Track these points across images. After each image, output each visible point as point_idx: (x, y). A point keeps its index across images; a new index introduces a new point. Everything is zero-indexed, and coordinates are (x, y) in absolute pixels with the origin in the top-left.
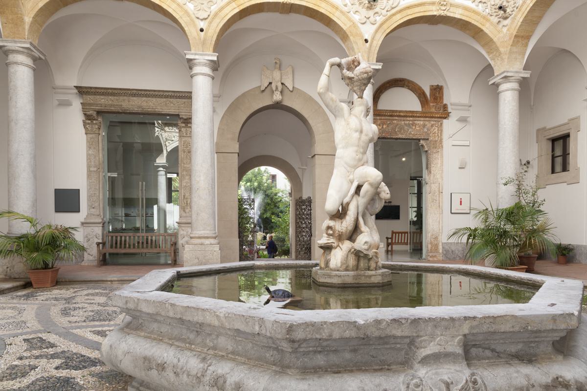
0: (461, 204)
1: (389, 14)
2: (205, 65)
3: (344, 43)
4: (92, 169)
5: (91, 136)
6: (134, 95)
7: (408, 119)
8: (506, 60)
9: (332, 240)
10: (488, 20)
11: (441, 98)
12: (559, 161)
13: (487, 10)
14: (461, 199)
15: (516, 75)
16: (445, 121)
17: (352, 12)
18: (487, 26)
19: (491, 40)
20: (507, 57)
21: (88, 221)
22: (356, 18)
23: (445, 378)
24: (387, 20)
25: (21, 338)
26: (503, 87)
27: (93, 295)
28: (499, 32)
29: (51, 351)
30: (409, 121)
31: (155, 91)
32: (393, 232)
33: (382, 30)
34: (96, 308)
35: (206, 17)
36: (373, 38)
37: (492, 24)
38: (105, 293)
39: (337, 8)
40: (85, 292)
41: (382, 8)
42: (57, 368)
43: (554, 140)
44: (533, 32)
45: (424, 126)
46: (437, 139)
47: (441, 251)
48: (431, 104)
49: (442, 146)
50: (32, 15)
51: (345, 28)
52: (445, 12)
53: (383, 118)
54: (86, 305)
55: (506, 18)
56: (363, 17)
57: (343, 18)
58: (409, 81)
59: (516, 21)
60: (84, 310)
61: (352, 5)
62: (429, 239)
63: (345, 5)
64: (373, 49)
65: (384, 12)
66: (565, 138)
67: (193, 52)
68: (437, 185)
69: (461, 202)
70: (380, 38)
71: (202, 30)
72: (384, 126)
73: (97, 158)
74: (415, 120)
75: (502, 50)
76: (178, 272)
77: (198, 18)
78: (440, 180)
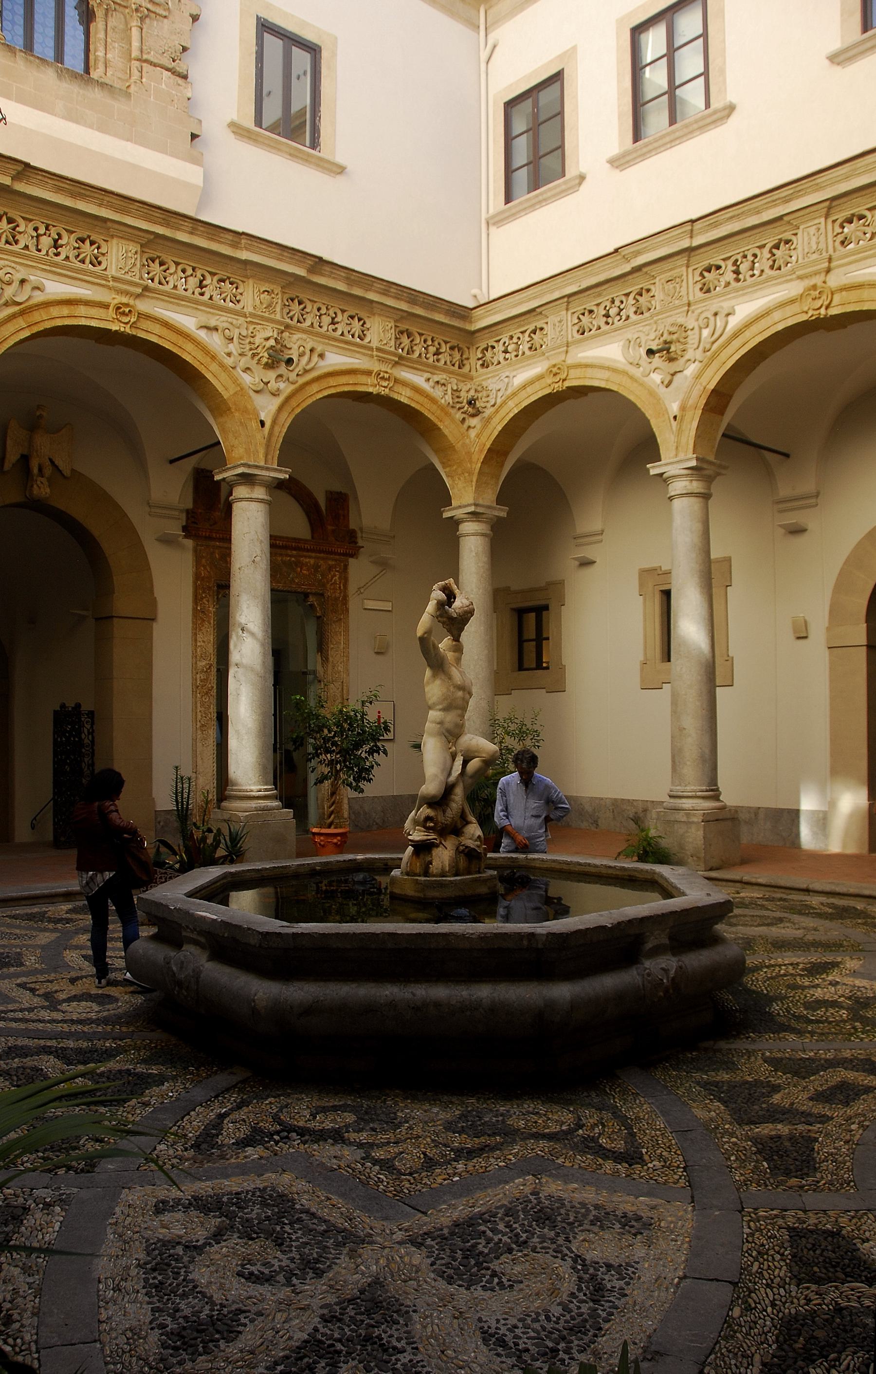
1: (301, 381)
3: (215, 418)
7: (289, 552)
9: (433, 836)
10: (447, 414)
11: (346, 517)
12: (530, 647)
14: (379, 712)
15: (488, 511)
16: (351, 560)
18: (446, 423)
19: (452, 447)
22: (247, 379)
23: (663, 966)
30: (291, 556)
39: (213, 358)
43: (520, 613)
44: (511, 447)
45: (317, 567)
46: (337, 595)
47: (346, 815)
48: (330, 528)
49: (347, 610)
51: (226, 395)
56: (257, 380)
57: (223, 376)
59: (491, 427)
63: (229, 355)
66: (541, 610)
68: (338, 684)
70: (286, 420)
74: (302, 557)
76: (225, 902)
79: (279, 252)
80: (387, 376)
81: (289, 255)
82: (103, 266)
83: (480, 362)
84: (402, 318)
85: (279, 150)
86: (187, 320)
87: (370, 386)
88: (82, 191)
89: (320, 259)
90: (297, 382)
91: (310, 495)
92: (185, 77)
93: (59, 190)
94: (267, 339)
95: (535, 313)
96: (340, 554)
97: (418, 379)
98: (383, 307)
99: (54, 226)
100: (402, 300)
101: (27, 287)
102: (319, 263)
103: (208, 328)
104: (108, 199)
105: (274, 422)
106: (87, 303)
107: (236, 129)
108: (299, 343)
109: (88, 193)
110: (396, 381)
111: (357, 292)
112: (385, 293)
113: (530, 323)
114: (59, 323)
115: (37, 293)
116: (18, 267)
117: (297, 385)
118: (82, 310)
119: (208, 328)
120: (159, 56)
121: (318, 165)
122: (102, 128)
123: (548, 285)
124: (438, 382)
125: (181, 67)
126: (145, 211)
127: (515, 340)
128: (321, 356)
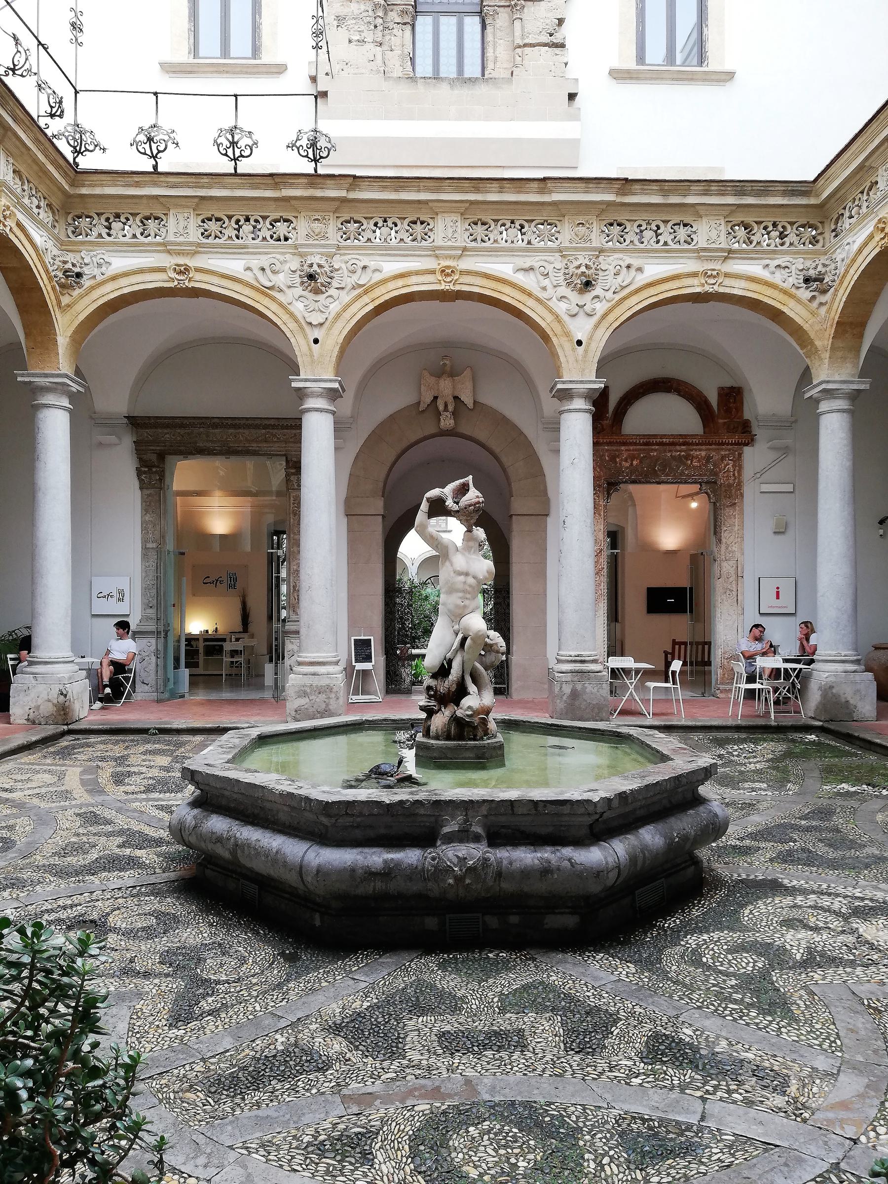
0: (778, 597)
1: (617, 297)
2: (320, 395)
4: (150, 545)
5: (148, 492)
6: (215, 426)
7: (678, 448)
8: (826, 361)
11: (740, 408)
13: (791, 279)
14: (778, 588)
15: (844, 386)
16: (746, 449)
17: (554, 299)
20: (828, 355)
21: (143, 629)
22: (561, 308)
24: (610, 310)
25: (70, 812)
26: (824, 406)
27: (150, 752)
28: (813, 314)
29: (109, 828)
31: (247, 419)
32: (674, 643)
33: (605, 324)
34: (155, 772)
35: (322, 321)
36: (591, 338)
37: (799, 301)
38: (169, 750)
39: (530, 295)
40: (142, 749)
41: (606, 288)
42: (119, 846)
48: (721, 421)
49: (742, 495)
50: (69, 334)
52: (716, 287)
53: (631, 448)
54: (144, 769)
55: (824, 292)
57: (540, 309)
58: (680, 382)
60: (142, 776)
61: (555, 287)
62: (718, 660)
63: (544, 289)
64: (590, 354)
65: (609, 295)
67: (302, 376)
69: (778, 593)
71: (316, 341)
72: (635, 463)
73: (158, 528)
75: (818, 343)
77: (310, 324)
78: (738, 555)
79: (584, 185)
80: (715, 273)
81: (595, 186)
82: (430, 240)
83: (834, 234)
84: (732, 212)
85: (662, 79)
87: (696, 286)
88: (402, 184)
89: (626, 180)
91: (700, 394)
92: (562, 46)
94: (579, 267)
95: (866, 169)
96: (732, 444)
97: (755, 269)
98: (706, 207)
100: (728, 194)
102: (625, 184)
103: (525, 270)
106: (417, 273)
107: (619, 75)
109: (406, 184)
110: (727, 275)
111: (674, 200)
112: (706, 193)
113: (865, 181)
115: (377, 274)
118: (414, 279)
119: (525, 270)
120: (536, 36)
121: (705, 80)
122: (487, 117)
123: (868, 134)
124: (778, 266)
125: (556, 39)
127: (856, 203)
128: (640, 270)
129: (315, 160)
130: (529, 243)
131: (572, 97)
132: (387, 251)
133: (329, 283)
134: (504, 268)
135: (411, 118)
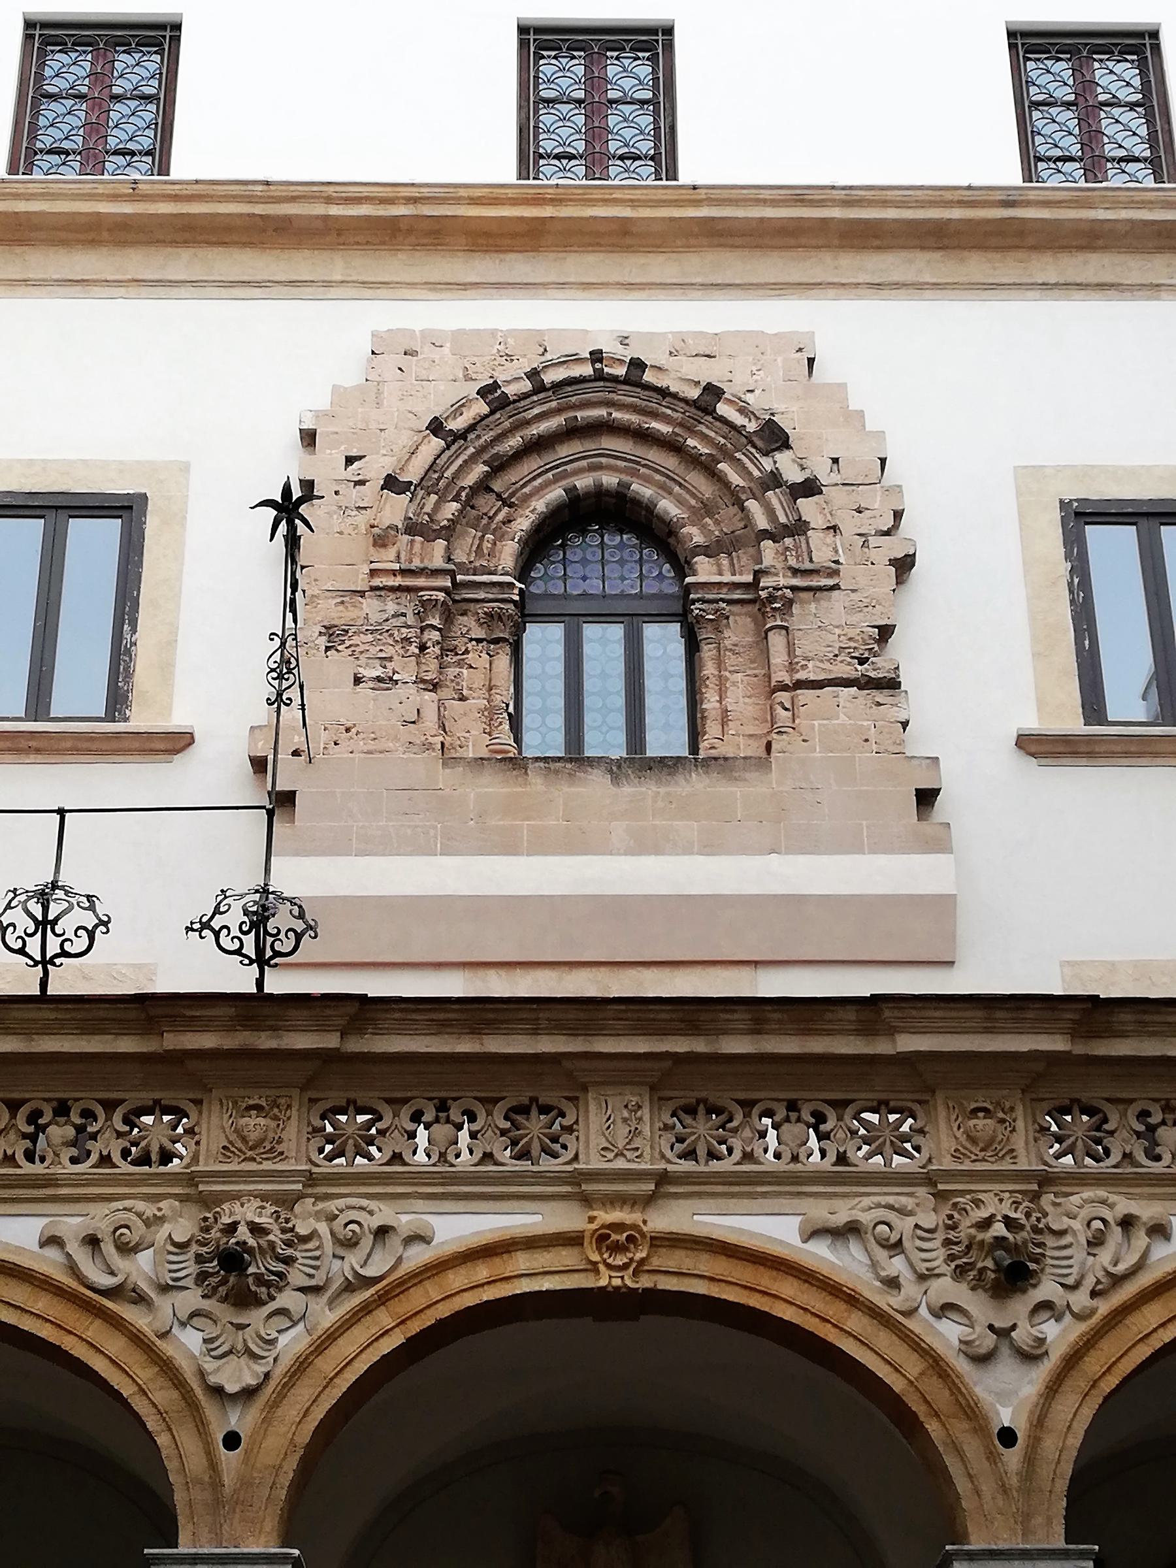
1: (1104, 1307)
39: (852, 1300)
70: (1075, 1415)
86: (776, 1222)
90: (1093, 1311)
92: (891, 684)
93: (441, 1028)
94: (986, 1224)
99: (455, 1099)
101: (394, 1242)
104: (547, 1015)
105: (1040, 1420)
106: (532, 1243)
107: (1036, 746)
108: (1085, 1213)
114: (469, 1300)
116: (372, 1205)
117: (1094, 1320)
118: (522, 1261)
120: (827, 665)
122: (710, 847)
125: (879, 668)
126: (635, 1016)
129: (261, 961)
130: (842, 1159)
131: (926, 798)
132: (448, 1186)
133: (281, 1275)
134: (776, 1228)
135: (511, 849)
